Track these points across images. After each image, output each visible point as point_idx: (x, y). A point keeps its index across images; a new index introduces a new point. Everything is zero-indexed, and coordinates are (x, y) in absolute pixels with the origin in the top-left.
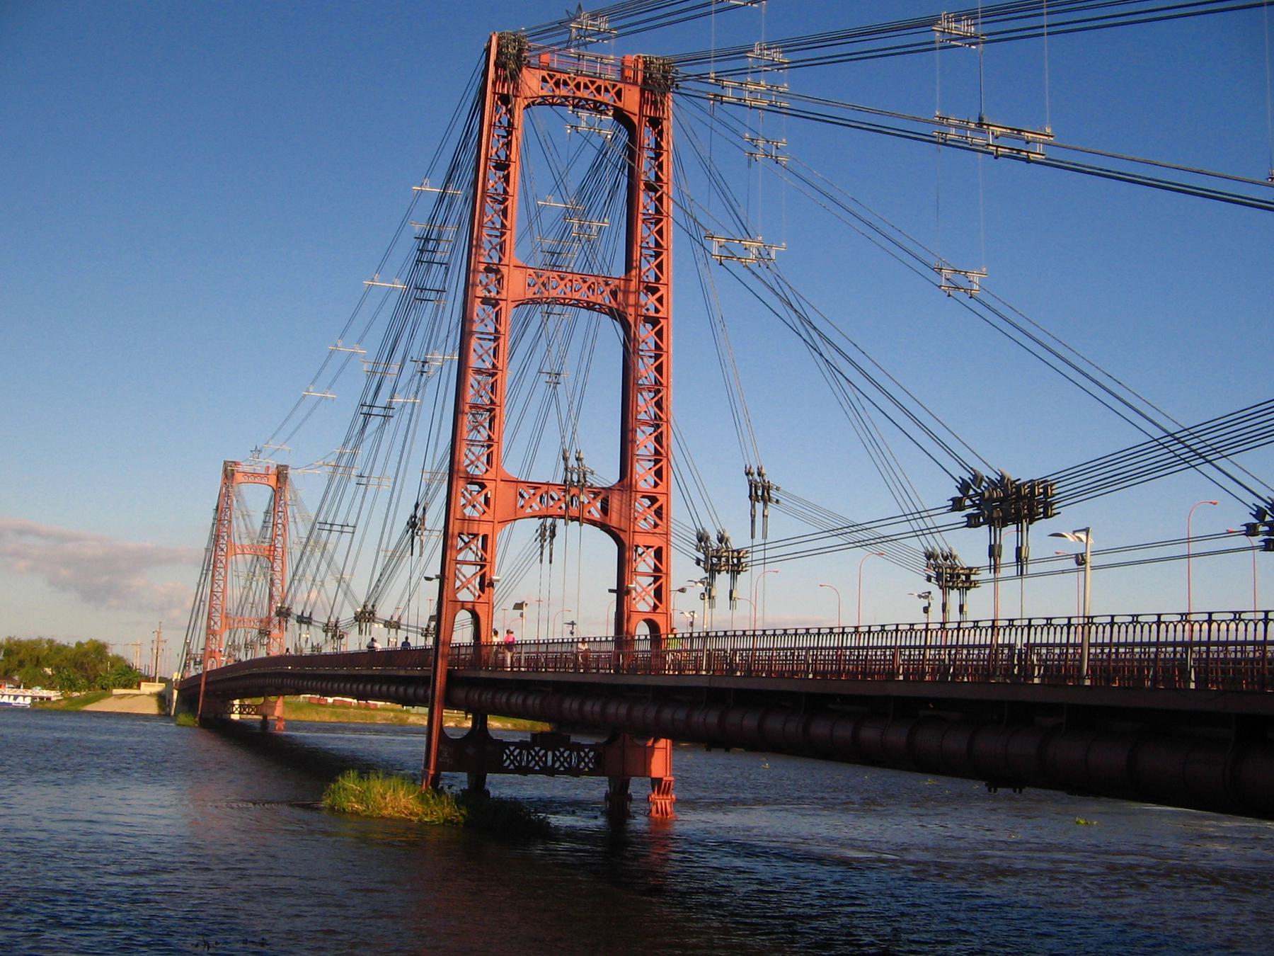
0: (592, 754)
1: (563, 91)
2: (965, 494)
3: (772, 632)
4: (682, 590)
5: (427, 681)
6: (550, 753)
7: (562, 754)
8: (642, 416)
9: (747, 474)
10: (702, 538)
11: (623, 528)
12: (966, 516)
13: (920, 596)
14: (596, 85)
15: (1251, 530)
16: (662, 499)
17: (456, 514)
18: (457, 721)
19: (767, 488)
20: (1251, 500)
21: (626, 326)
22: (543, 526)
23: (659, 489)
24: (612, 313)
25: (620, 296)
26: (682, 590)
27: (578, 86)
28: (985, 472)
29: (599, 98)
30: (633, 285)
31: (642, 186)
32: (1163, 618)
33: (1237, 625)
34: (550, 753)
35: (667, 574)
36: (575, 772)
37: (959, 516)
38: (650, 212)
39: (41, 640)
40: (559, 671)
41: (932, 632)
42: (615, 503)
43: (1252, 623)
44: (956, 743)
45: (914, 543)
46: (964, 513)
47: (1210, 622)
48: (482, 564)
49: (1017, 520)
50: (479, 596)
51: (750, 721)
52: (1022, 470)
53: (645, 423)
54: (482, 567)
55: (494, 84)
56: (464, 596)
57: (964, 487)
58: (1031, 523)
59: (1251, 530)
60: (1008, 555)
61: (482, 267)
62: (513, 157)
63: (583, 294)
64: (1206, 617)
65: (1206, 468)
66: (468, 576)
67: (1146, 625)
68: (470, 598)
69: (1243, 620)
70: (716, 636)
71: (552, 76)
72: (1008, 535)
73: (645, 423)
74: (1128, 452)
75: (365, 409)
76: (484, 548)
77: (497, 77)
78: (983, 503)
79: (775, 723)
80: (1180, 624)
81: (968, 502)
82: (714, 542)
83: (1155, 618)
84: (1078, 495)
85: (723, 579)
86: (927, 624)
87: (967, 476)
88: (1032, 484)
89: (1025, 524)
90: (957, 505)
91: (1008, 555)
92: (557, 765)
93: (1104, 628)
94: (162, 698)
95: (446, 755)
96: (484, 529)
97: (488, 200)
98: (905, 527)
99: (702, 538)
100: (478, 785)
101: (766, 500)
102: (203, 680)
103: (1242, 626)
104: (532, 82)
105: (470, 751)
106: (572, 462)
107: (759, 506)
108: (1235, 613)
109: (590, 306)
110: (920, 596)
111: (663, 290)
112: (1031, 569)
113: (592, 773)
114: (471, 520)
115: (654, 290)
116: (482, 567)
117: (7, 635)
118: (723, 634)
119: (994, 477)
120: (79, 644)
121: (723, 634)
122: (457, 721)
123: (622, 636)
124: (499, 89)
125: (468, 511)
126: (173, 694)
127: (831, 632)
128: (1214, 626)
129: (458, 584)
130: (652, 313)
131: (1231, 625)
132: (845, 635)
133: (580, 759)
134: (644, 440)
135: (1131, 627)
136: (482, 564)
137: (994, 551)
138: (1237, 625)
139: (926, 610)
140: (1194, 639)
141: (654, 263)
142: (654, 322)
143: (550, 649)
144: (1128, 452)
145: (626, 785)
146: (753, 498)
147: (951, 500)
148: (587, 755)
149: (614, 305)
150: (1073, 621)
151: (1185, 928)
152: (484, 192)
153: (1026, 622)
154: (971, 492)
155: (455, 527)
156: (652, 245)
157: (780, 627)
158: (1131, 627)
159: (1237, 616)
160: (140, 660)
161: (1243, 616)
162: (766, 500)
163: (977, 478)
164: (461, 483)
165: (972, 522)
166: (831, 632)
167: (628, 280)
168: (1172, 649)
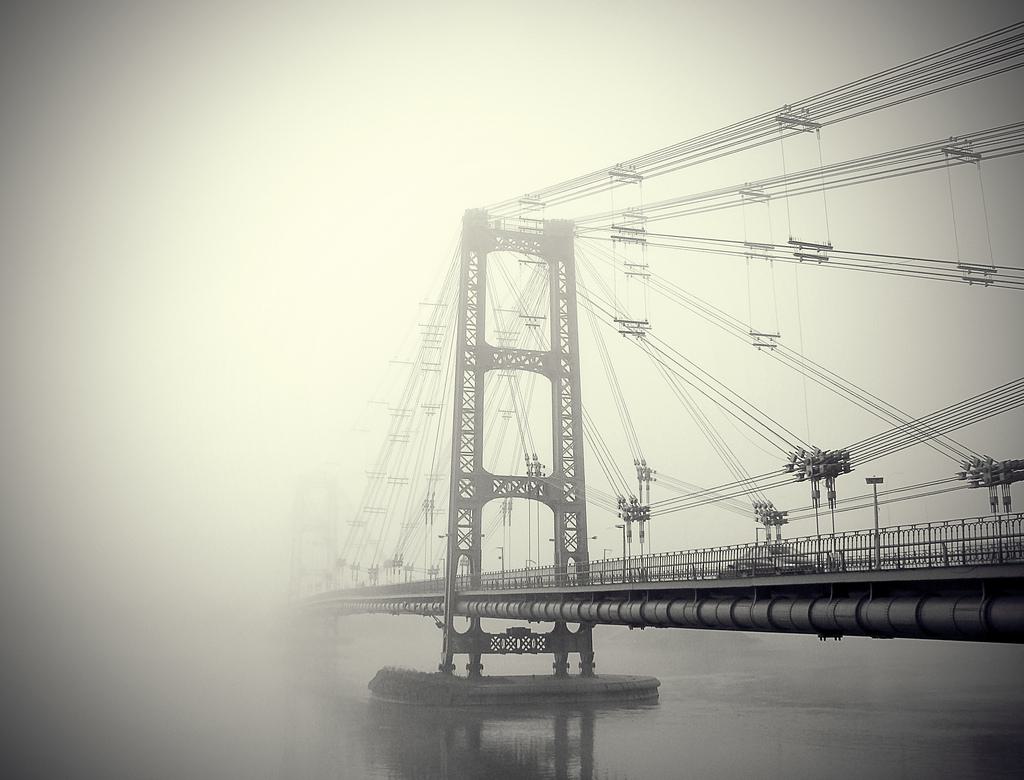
0: (544, 640)
4: (594, 538)
6: (519, 640)
7: (526, 640)
10: (622, 501)
15: (963, 476)
19: (649, 471)
20: (960, 458)
22: (505, 503)
26: (594, 538)
34: (519, 640)
36: (534, 651)
40: (903, 569)
44: (800, 610)
45: (745, 499)
46: (795, 473)
51: (662, 607)
52: (830, 445)
59: (963, 476)
65: (930, 442)
75: (392, 438)
79: (678, 608)
83: (927, 526)
84: (867, 458)
86: (819, 536)
87: (794, 451)
92: (523, 647)
98: (740, 489)
99: (622, 501)
101: (648, 479)
105: (471, 640)
106: (531, 461)
107: (644, 483)
112: (839, 507)
113: (544, 651)
120: (409, 670)
123: (560, 568)
133: (537, 643)
146: (640, 478)
148: (541, 640)
154: (798, 460)
157: (664, 552)
162: (648, 479)
165: (801, 478)
168: (882, 550)
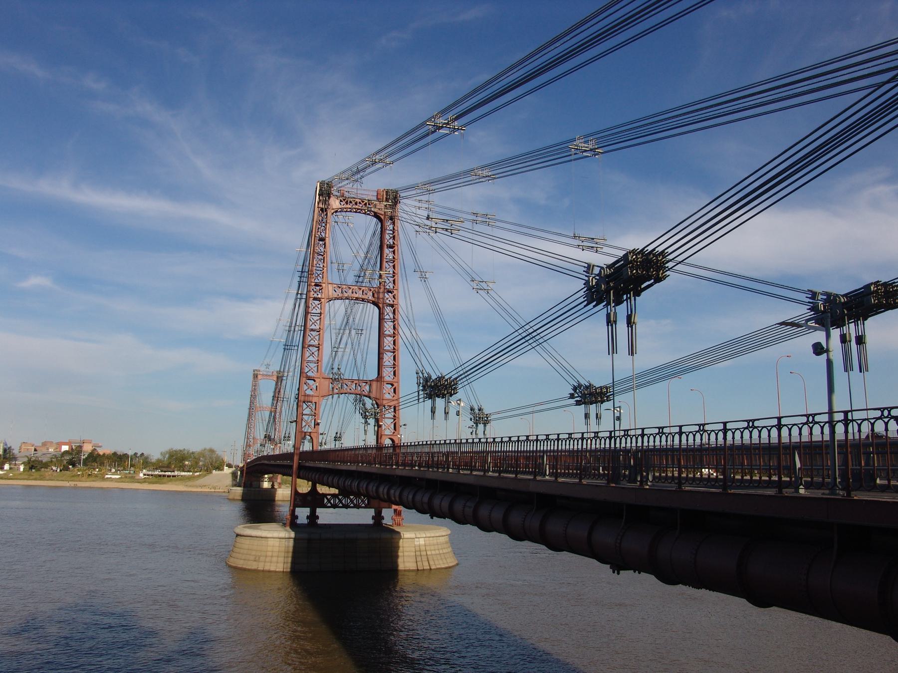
1: (349, 206)
2: (575, 391)
8: (387, 348)
9: (417, 373)
10: (472, 409)
11: (378, 398)
12: (576, 401)
13: (469, 427)
14: (364, 203)
16: (395, 385)
17: (302, 393)
18: (304, 487)
23: (394, 380)
25: (376, 295)
27: (356, 204)
28: (583, 382)
29: (357, 207)
30: (381, 290)
31: (385, 246)
35: (398, 418)
37: (572, 401)
38: (391, 258)
41: (562, 441)
43: (652, 436)
46: (575, 400)
50: (394, 433)
53: (388, 351)
54: (395, 420)
55: (318, 203)
57: (575, 389)
58: (602, 403)
61: (313, 284)
62: (327, 236)
63: (359, 295)
66: (389, 424)
67: (652, 436)
68: (310, 430)
71: (345, 200)
72: (593, 407)
73: (388, 351)
76: (395, 411)
77: (320, 200)
78: (584, 396)
81: (576, 395)
82: (477, 411)
87: (576, 384)
89: (599, 404)
90: (572, 396)
94: (234, 474)
95: (298, 500)
96: (315, 400)
97: (316, 254)
99: (472, 409)
103: (664, 437)
104: (335, 203)
110: (469, 427)
111: (395, 292)
113: (366, 507)
114: (309, 396)
116: (395, 420)
119: (587, 384)
122: (304, 487)
124: (321, 206)
126: (237, 473)
128: (684, 436)
130: (391, 302)
132: (560, 441)
134: (388, 358)
139: (472, 433)
140: (783, 441)
141: (391, 279)
143: (463, 449)
145: (381, 512)
147: (570, 394)
149: (373, 299)
152: (314, 251)
154: (578, 391)
155: (302, 398)
156: (391, 272)
160: (227, 459)
163: (580, 386)
164: (304, 379)
165: (578, 403)
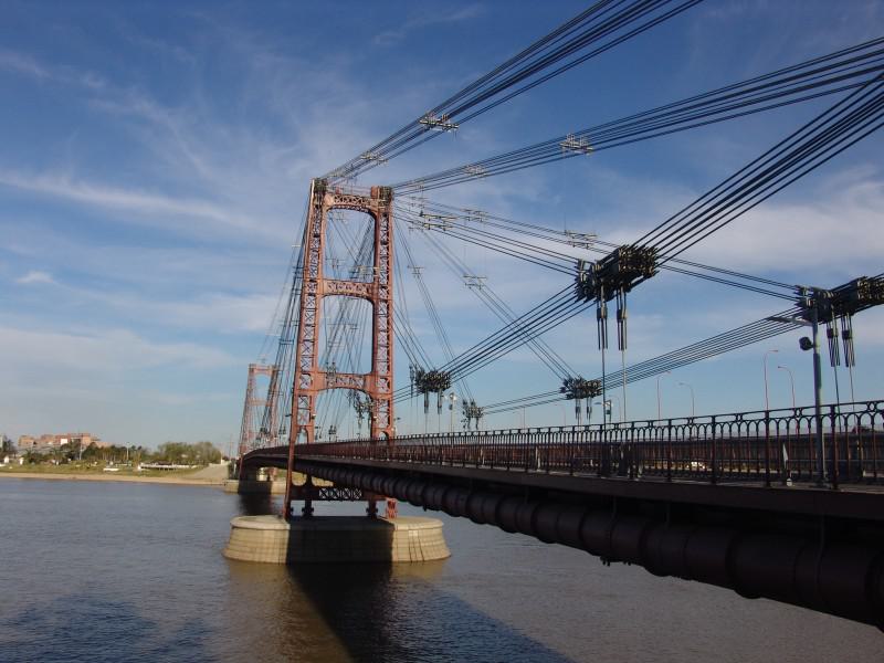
3: (547, 431)
5: (286, 460)
18: (299, 479)
21: (373, 303)
24: (368, 299)
32: (717, 420)
33: (739, 426)
37: (563, 395)
39: (202, 443)
42: (368, 379)
47: (670, 427)
48: (388, 412)
49: (587, 396)
56: (381, 426)
57: (566, 383)
60: (584, 410)
63: (354, 290)
64: (763, 416)
69: (804, 417)
70: (494, 435)
72: (584, 401)
74: (781, 148)
76: (389, 405)
78: (574, 390)
80: (866, 415)
82: (469, 405)
83: (710, 420)
85: (473, 420)
88: (592, 382)
90: (563, 390)
91: (584, 410)
93: (705, 428)
99: (465, 403)
100: (308, 509)
102: (291, 452)
108: (737, 415)
109: (357, 295)
115: (385, 288)
117: (205, 439)
118: (516, 432)
121: (516, 432)
122: (299, 479)
125: (304, 386)
127: (539, 432)
129: (299, 417)
131: (790, 424)
134: (382, 353)
135: (647, 431)
136: (388, 412)
137: (578, 410)
138: (739, 426)
140: (771, 434)
142: (386, 301)
144: (781, 148)
150: (576, 429)
151: (351, 170)
153: (629, 426)
155: (297, 392)
158: (647, 431)
159: (872, 407)
160: (223, 452)
161: (744, 417)
163: (571, 380)
165: (569, 397)
166: (539, 432)
167: (373, 283)
